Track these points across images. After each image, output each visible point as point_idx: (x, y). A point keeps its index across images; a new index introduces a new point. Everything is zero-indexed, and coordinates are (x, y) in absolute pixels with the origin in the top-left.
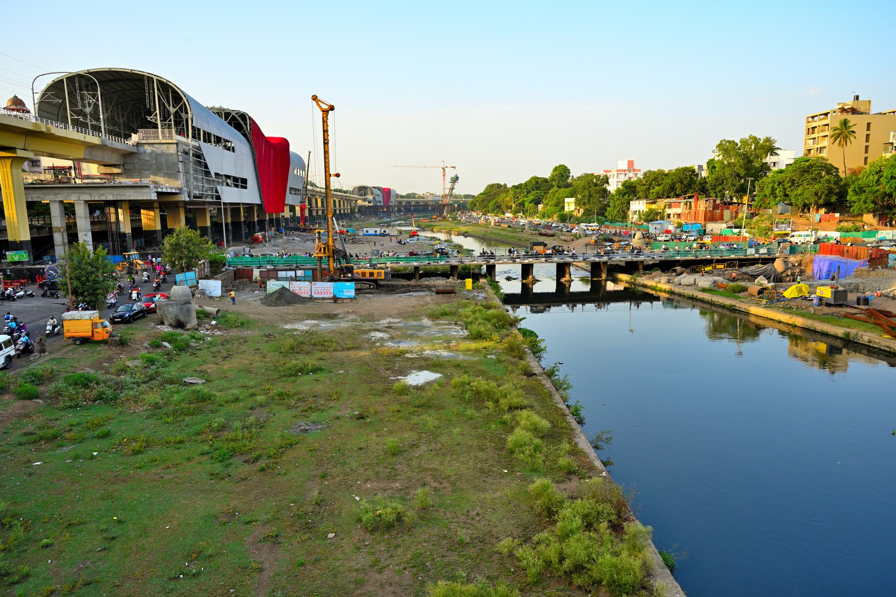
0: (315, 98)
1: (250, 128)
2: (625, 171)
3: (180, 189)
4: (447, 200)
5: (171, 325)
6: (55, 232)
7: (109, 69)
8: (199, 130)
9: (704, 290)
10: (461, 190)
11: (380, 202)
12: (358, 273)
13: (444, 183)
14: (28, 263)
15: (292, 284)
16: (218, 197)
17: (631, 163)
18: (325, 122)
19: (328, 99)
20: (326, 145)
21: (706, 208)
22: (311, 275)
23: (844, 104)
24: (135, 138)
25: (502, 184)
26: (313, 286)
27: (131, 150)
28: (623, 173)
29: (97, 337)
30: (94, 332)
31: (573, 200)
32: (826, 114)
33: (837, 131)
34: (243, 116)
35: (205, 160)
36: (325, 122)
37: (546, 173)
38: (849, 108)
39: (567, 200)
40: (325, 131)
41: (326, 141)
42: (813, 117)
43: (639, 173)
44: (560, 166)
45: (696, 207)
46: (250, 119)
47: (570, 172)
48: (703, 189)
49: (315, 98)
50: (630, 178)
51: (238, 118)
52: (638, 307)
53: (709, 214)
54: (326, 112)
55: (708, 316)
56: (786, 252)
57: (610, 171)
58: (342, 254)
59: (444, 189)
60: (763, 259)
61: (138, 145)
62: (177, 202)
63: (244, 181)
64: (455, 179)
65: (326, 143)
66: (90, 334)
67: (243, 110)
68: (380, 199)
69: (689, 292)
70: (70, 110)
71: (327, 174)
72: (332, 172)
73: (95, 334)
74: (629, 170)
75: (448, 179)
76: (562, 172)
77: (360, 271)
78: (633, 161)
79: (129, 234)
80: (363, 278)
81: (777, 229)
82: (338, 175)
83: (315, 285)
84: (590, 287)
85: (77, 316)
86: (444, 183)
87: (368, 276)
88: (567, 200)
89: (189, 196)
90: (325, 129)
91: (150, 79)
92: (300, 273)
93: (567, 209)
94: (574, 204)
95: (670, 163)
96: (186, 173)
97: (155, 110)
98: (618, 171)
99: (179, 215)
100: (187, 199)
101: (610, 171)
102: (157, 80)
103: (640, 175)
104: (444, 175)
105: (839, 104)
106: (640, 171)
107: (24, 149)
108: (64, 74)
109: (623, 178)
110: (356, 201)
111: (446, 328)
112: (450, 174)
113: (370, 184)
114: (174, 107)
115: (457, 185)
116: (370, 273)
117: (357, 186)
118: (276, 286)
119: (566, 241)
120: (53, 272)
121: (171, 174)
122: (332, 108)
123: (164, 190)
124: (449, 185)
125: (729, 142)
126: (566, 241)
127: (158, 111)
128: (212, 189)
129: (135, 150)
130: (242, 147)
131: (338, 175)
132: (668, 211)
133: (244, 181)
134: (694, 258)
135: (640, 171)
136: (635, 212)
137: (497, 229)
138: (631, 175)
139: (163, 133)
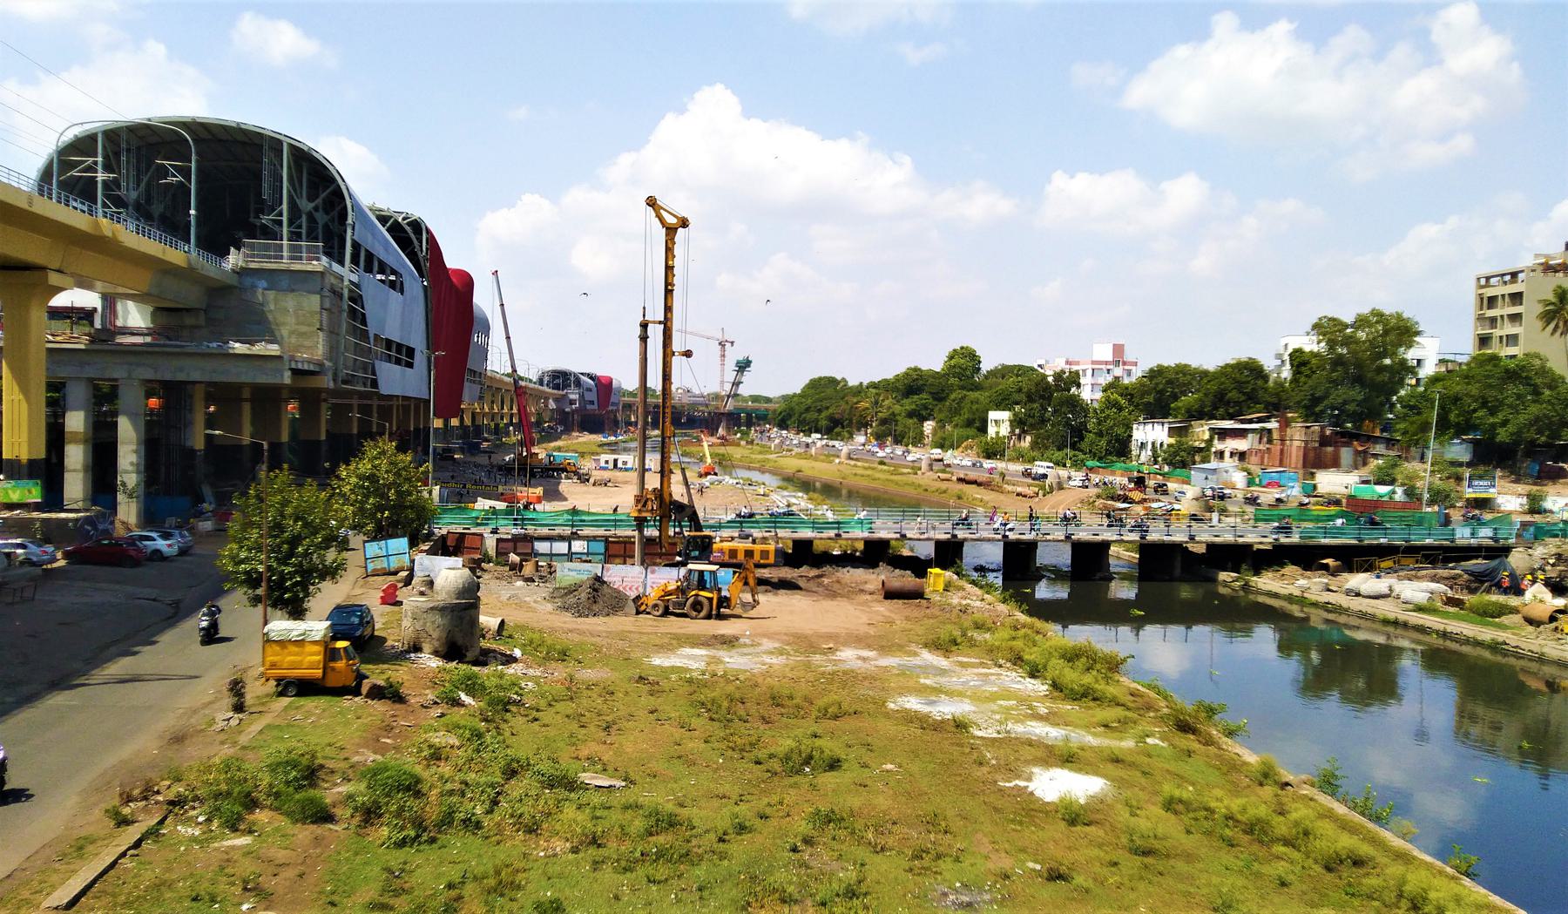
0: (652, 202)
1: (427, 249)
2: (1106, 363)
3: (321, 365)
4: (730, 406)
5: (436, 653)
6: (70, 442)
7: (238, 124)
8: (359, 245)
9: (1420, 609)
10: (751, 386)
11: (592, 403)
12: (721, 551)
13: (723, 370)
14: (37, 507)
15: (608, 570)
16: (375, 383)
17: (1118, 349)
18: (669, 250)
19: (677, 204)
20: (669, 296)
21: (1306, 442)
22: (603, 551)
23: (1546, 256)
24: (234, 259)
25: (839, 378)
26: (649, 575)
27: (229, 282)
28: (1103, 367)
29: (332, 682)
30: (329, 670)
31: (1005, 415)
32: (1514, 275)
33: (1551, 307)
34: (417, 226)
35: (363, 308)
36: (669, 250)
37: (934, 362)
38: (1559, 265)
39: (993, 415)
40: (669, 269)
41: (670, 287)
42: (1488, 279)
43: (1133, 368)
44: (962, 348)
45: (1283, 440)
46: (428, 231)
47: (980, 362)
48: (1276, 404)
49: (652, 202)
50: (1117, 378)
51: (408, 229)
52: (1137, 635)
53: (1312, 454)
54: (671, 231)
55: (1296, 656)
56: (1528, 536)
57: (1078, 363)
58: (688, 511)
59: (722, 382)
60: (1488, 549)
61: (242, 272)
62: (319, 391)
63: (411, 352)
64: (743, 366)
65: (668, 292)
66: (318, 673)
67: (416, 213)
68: (592, 396)
69: (1386, 609)
70: (105, 195)
71: (668, 351)
72: (677, 345)
73: (330, 675)
74: (1117, 363)
75: (731, 366)
76: (963, 362)
77: (727, 545)
78: (1114, 345)
79: (200, 451)
80: (731, 561)
81: (1471, 490)
82: (688, 354)
83: (653, 572)
84: (1136, 591)
85: (295, 633)
86: (723, 370)
87: (741, 557)
88: (993, 415)
89: (334, 380)
90: (670, 263)
91: (275, 143)
92: (578, 546)
93: (992, 430)
94: (1008, 423)
95: (1210, 355)
96: (331, 332)
97: (281, 204)
98: (1094, 362)
99: (240, 415)
100: (331, 385)
101: (1078, 363)
102: (291, 145)
103: (1138, 373)
104: (723, 356)
105: (1537, 256)
106: (1135, 364)
107: (58, 271)
108: (100, 124)
109: (1105, 380)
110: (546, 399)
111: (992, 674)
112: (734, 355)
113: (574, 366)
114: (311, 199)
115: (747, 377)
116: (762, 551)
117: (550, 369)
118: (574, 573)
119: (1025, 496)
120: (89, 528)
121: (305, 333)
122: (684, 223)
123: (300, 366)
124: (731, 376)
125: (1330, 319)
126: (1025, 496)
127: (285, 206)
128: (365, 367)
129: (234, 281)
130: (415, 285)
131: (688, 354)
132: (1218, 445)
133: (411, 352)
134: (1354, 542)
135: (1135, 364)
136: (1143, 446)
137: (855, 466)
138: (1118, 372)
139: (293, 249)
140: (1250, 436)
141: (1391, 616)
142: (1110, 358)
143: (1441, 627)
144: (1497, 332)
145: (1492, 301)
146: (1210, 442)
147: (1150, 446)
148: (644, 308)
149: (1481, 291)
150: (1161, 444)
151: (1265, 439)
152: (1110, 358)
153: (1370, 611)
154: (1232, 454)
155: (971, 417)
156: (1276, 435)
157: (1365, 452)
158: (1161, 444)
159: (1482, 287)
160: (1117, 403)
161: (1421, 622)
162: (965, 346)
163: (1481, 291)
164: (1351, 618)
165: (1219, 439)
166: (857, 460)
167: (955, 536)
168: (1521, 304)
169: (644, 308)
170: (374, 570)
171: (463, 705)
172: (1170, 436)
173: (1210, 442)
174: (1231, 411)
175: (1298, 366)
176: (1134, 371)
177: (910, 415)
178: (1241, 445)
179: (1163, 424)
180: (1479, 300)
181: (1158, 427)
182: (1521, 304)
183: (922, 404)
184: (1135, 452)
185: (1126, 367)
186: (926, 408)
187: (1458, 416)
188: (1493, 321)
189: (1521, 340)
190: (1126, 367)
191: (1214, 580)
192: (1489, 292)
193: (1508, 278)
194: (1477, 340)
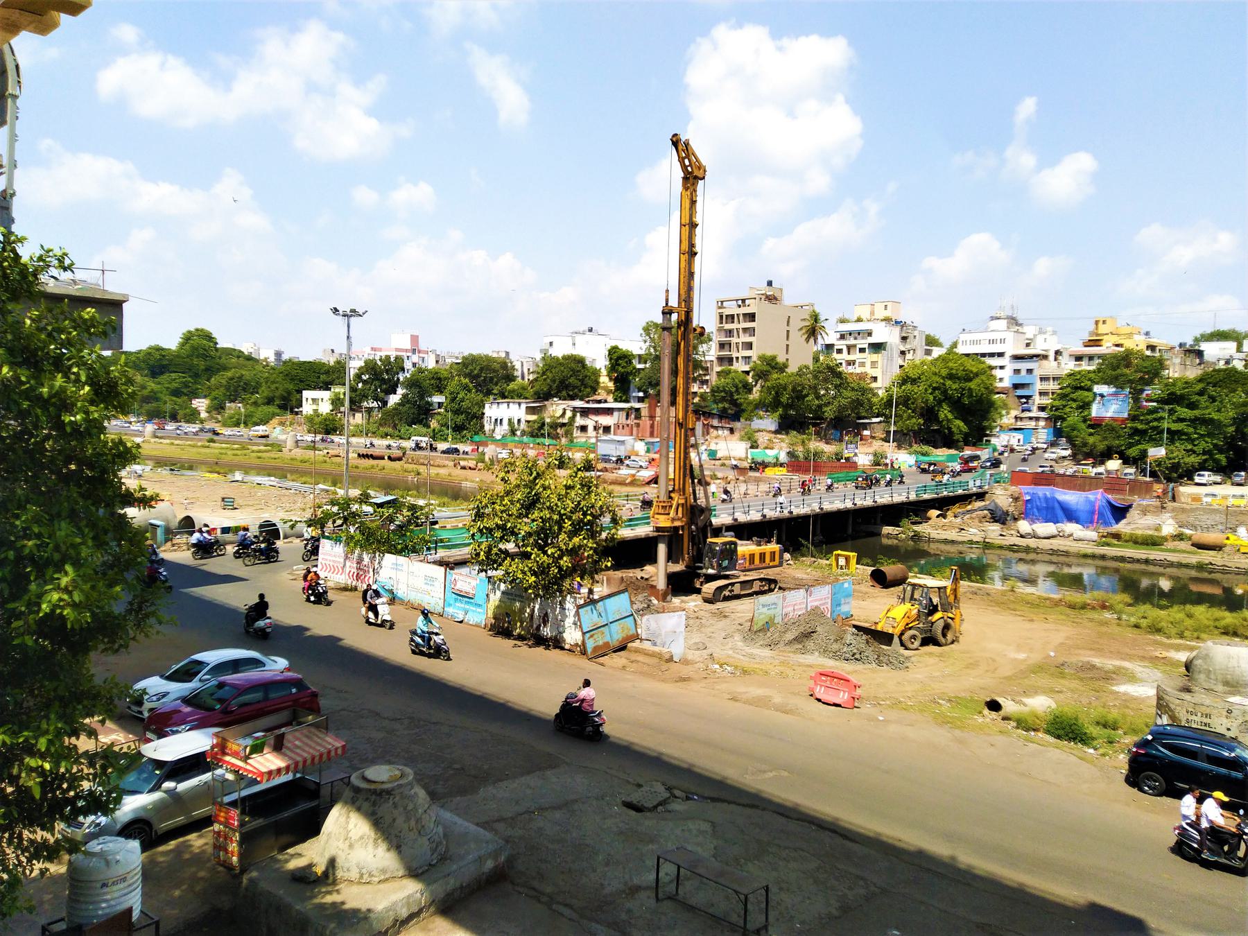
2: (406, 351)
17: (415, 339)
44: (197, 330)
74: (414, 351)
78: (418, 336)
140: (616, 414)
141: (1089, 551)
142: (409, 347)
143: (1144, 557)
144: (734, 340)
145: (731, 318)
146: (573, 418)
147: (505, 422)
148: (667, 291)
149: (721, 311)
150: (519, 421)
151: (633, 416)
152: (409, 347)
153: (1062, 548)
154: (595, 428)
155: (271, 395)
156: (645, 413)
157: (708, 424)
158: (519, 421)
159: (720, 308)
160: (467, 386)
161: (1120, 554)
162: (199, 327)
163: (721, 311)
164: (1040, 555)
165: (581, 415)
166: (161, 438)
167: (764, 516)
168: (754, 321)
169: (667, 291)
170: (595, 649)
171: (389, 792)
172: (527, 413)
173: (573, 418)
174: (571, 393)
175: (617, 360)
176: (426, 359)
177: (176, 393)
178: (605, 420)
179: (519, 404)
180: (718, 317)
181: (514, 407)
182: (754, 321)
183: (182, 382)
184: (487, 427)
185: (421, 355)
186: (187, 386)
187: (788, 399)
188: (730, 333)
189: (754, 346)
190: (421, 355)
191: (879, 534)
192: (727, 312)
193: (740, 302)
194: (718, 345)
